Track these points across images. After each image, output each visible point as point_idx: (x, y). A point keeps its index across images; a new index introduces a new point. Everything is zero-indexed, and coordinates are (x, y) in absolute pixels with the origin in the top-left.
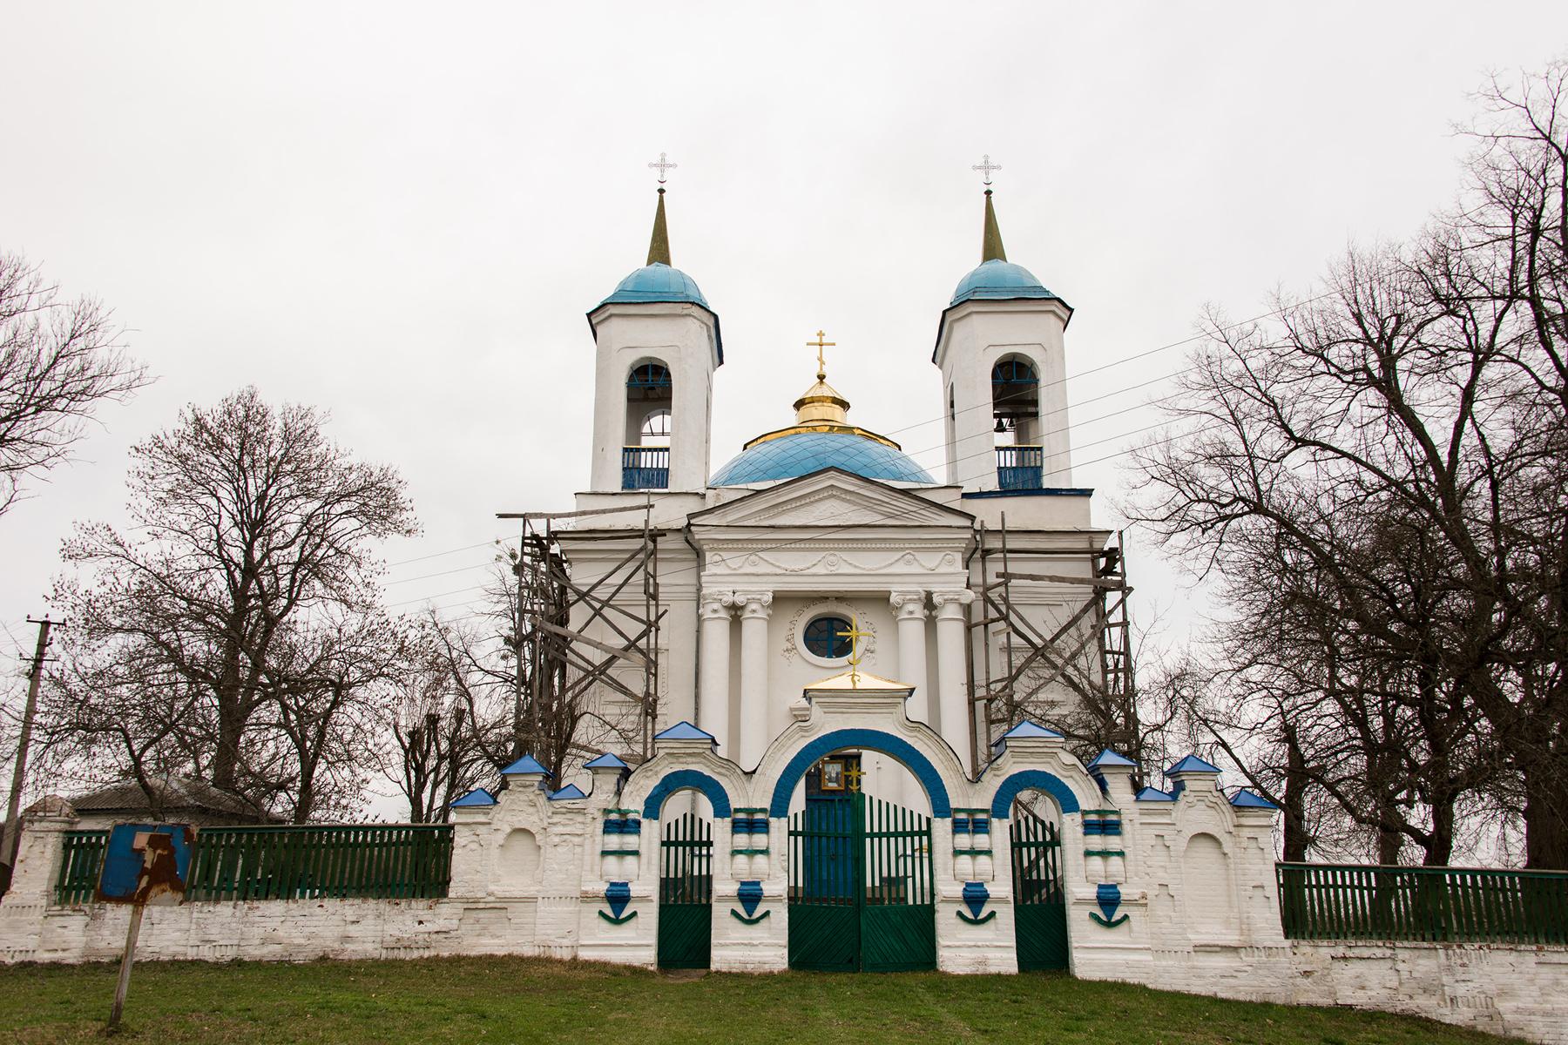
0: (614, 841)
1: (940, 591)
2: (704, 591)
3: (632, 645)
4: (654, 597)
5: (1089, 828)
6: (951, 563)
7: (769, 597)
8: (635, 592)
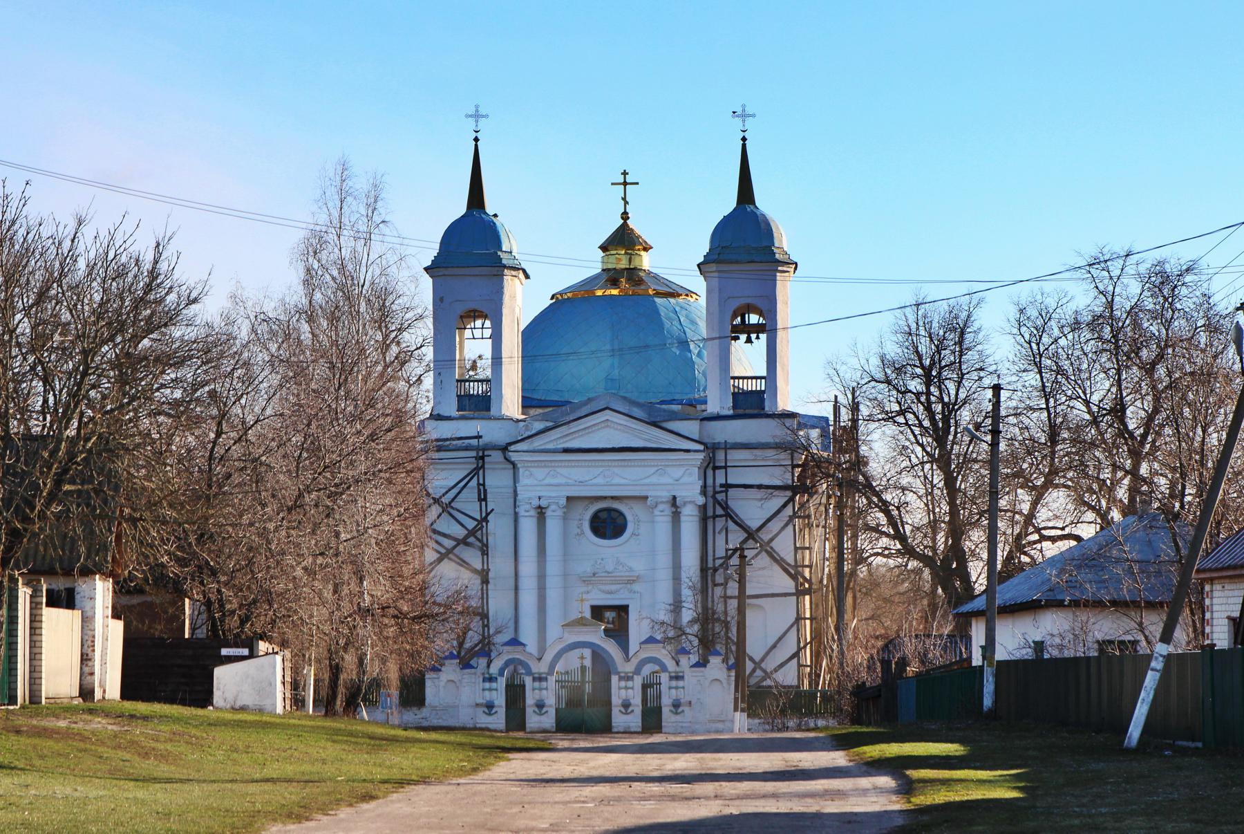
0: (487, 685)
1: (681, 494)
2: (519, 497)
3: (472, 533)
4: (485, 499)
5: (671, 678)
6: (690, 474)
7: (563, 502)
8: (471, 494)
